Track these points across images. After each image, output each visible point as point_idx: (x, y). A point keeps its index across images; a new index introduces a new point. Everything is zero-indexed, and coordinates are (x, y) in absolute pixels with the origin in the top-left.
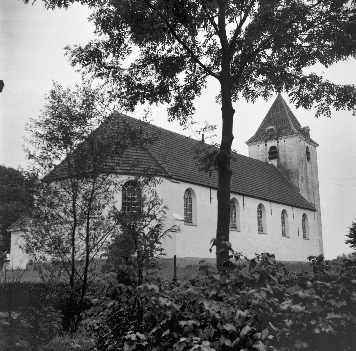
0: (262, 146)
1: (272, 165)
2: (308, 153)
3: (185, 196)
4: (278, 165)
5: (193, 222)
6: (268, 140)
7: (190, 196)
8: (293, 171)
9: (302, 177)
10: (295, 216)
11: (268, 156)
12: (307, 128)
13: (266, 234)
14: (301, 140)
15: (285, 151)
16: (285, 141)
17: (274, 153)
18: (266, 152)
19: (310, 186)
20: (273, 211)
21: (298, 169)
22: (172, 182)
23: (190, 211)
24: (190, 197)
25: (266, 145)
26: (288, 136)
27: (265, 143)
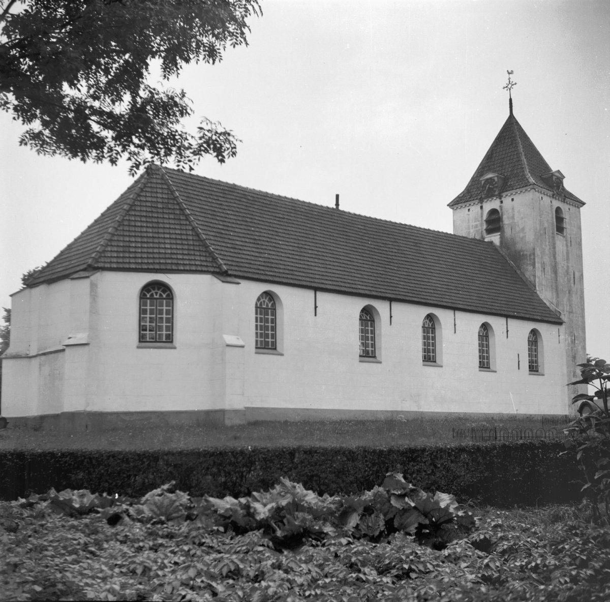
0: (475, 209)
1: (491, 242)
2: (559, 220)
3: (424, 324)
4: (501, 242)
5: (278, 348)
6: (485, 198)
8: (525, 253)
9: (543, 264)
11: (485, 227)
12: (557, 174)
13: (442, 367)
14: (543, 196)
15: (513, 217)
16: (513, 200)
17: (494, 222)
18: (482, 219)
19: (562, 280)
21: (534, 249)
22: (223, 282)
23: (433, 353)
24: (432, 325)
25: (481, 207)
26: (523, 190)
27: (480, 205)
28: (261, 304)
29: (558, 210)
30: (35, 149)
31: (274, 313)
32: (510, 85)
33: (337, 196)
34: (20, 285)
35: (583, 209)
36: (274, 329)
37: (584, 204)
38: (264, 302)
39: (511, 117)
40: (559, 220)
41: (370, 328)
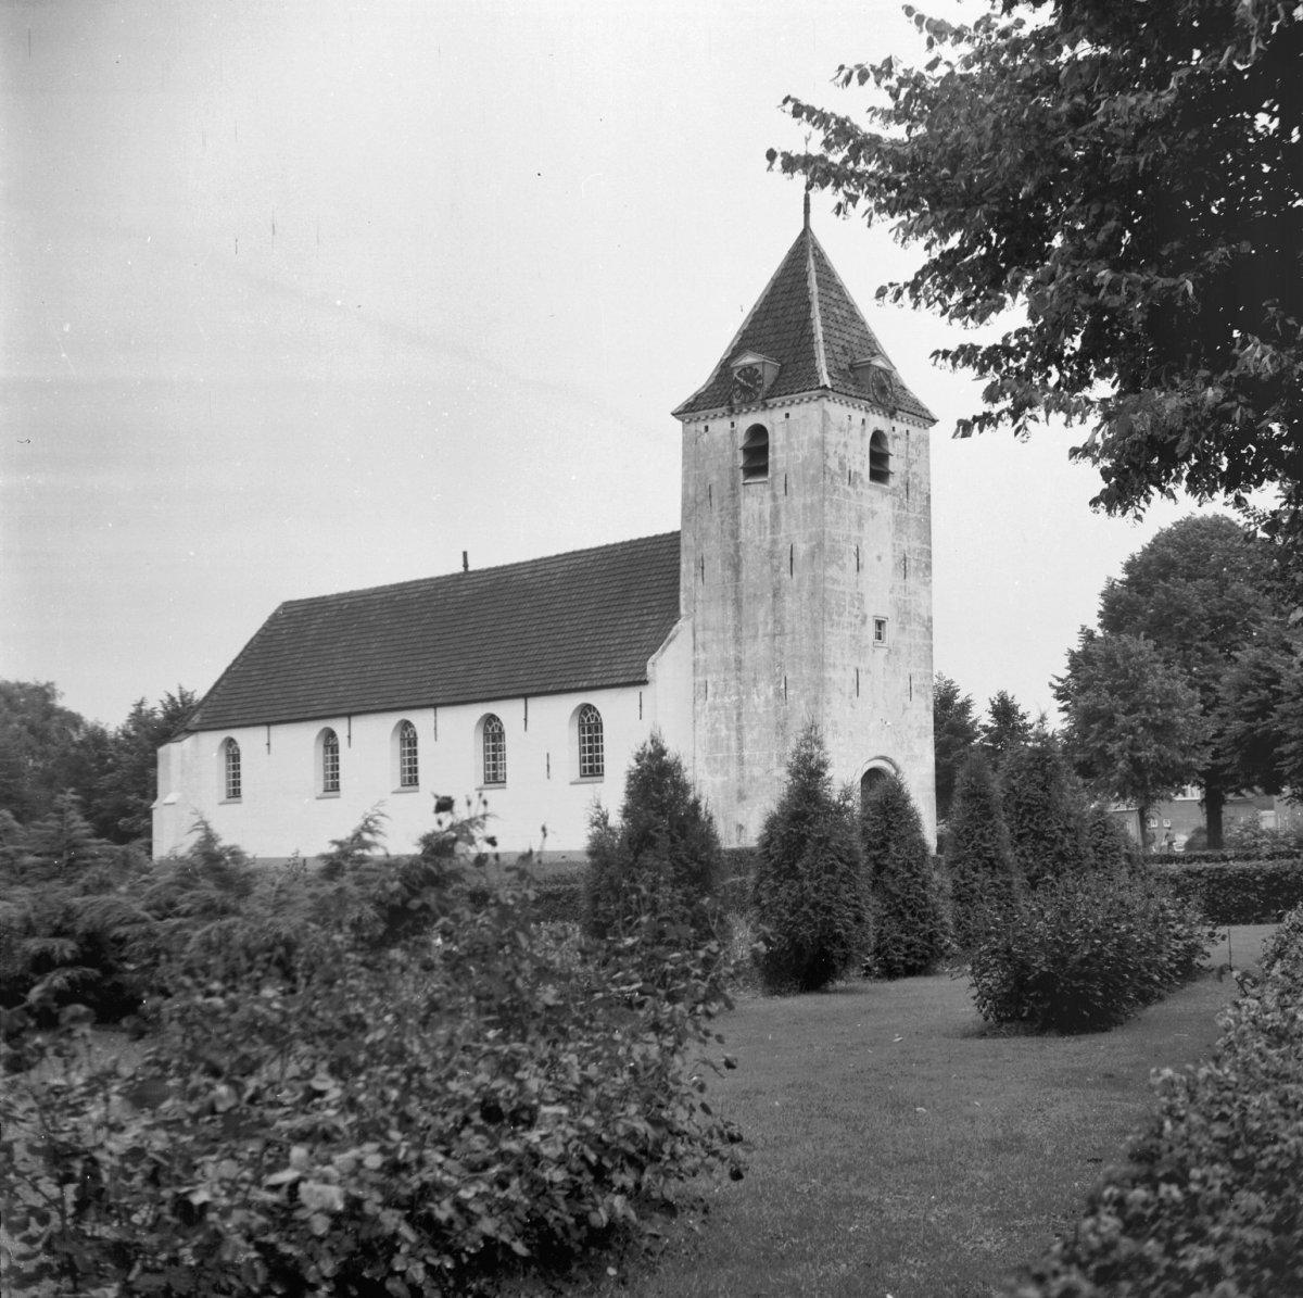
33: (465, 554)
34: (768, 163)
37: (934, 421)
39: (806, 230)
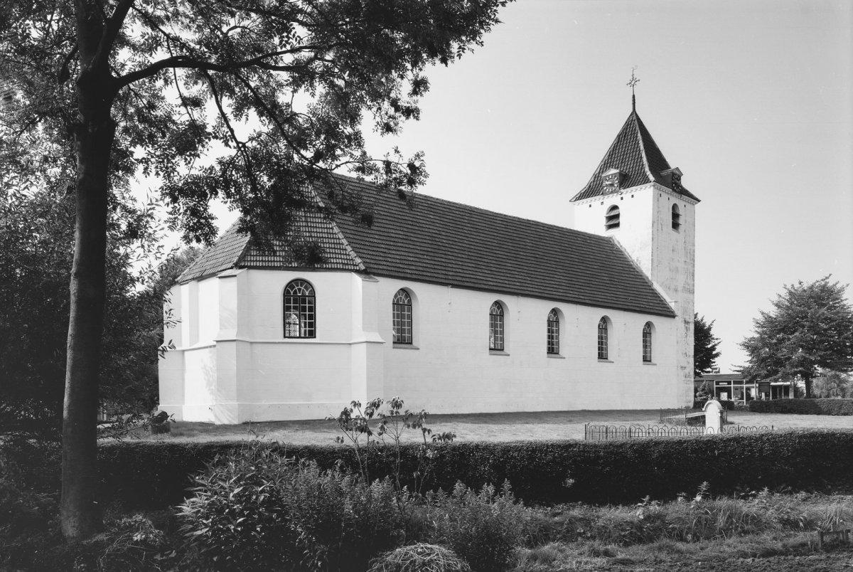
2: (675, 216)
3: (549, 318)
7: (606, 326)
10: (626, 326)
20: (580, 321)
24: (500, 313)
28: (398, 300)
29: (675, 207)
30: (437, 61)
31: (410, 310)
32: (633, 82)
35: (698, 206)
36: (410, 324)
37: (699, 201)
38: (401, 298)
40: (675, 216)
41: (406, 313)
